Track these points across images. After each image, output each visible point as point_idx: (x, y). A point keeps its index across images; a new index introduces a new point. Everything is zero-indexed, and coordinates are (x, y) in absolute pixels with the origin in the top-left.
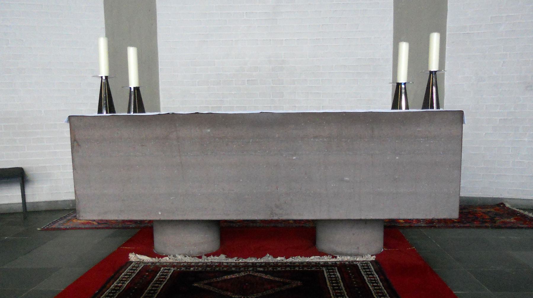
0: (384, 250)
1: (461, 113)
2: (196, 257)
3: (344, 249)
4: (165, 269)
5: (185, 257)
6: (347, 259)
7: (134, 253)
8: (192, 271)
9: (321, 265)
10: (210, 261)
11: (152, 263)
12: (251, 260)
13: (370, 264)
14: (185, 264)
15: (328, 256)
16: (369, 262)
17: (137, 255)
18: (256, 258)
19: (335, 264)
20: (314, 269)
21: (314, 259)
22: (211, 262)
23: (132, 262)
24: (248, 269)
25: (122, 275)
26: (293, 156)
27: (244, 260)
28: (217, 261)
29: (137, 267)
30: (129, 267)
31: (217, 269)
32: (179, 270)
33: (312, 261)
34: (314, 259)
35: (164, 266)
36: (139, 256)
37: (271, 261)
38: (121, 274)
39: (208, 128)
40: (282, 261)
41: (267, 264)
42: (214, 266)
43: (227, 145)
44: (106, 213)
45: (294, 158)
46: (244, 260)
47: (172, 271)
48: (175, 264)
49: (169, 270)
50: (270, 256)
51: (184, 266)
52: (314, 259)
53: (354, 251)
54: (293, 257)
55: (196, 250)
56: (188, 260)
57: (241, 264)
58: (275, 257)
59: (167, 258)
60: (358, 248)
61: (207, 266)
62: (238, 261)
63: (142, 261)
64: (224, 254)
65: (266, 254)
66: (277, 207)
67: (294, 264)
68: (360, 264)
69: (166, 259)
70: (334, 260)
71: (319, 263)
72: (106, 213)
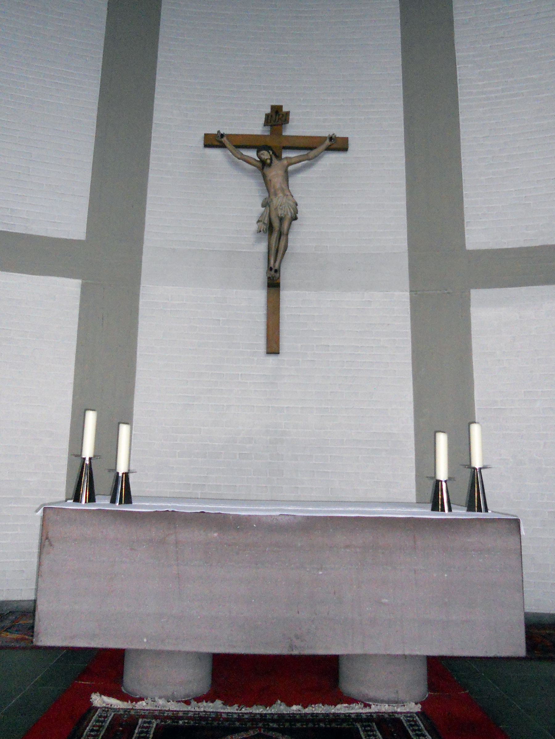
0: (429, 695)
1: (517, 522)
2: (183, 701)
3: (381, 694)
4: (145, 722)
5: (169, 702)
6: (385, 709)
7: (98, 694)
8: (182, 727)
9: (353, 719)
10: (202, 709)
11: (125, 710)
12: (258, 710)
13: (417, 718)
14: (170, 714)
15: (358, 704)
16: (415, 715)
17: (103, 696)
18: (264, 708)
19: (370, 718)
20: (345, 725)
21: (341, 709)
22: (204, 711)
23: (96, 709)
24: (257, 724)
25: (86, 731)
26: (318, 570)
27: (249, 710)
28: (212, 710)
29: (105, 717)
30: (94, 718)
31: (215, 723)
32: (163, 723)
33: (339, 712)
34: (341, 709)
35: (143, 717)
36: (105, 698)
37: (285, 712)
38: (85, 729)
39: (215, 532)
40: (299, 712)
41: (281, 717)
42: (210, 719)
43: (238, 554)
44: (73, 638)
45: (320, 573)
46: (249, 710)
47: (154, 725)
48: (157, 713)
49: (149, 723)
50: (282, 704)
51: (168, 717)
52: (341, 709)
53: (392, 696)
54: (313, 706)
55: (182, 691)
56: (173, 706)
57: (246, 716)
58: (289, 705)
59: (144, 703)
60: (397, 692)
61: (201, 718)
62: (241, 710)
63: (109, 706)
64: (220, 698)
65: (277, 700)
66: (297, 637)
67: (317, 716)
68: (403, 717)
69: (142, 705)
70: (367, 710)
71: (349, 715)
72: (73, 638)
